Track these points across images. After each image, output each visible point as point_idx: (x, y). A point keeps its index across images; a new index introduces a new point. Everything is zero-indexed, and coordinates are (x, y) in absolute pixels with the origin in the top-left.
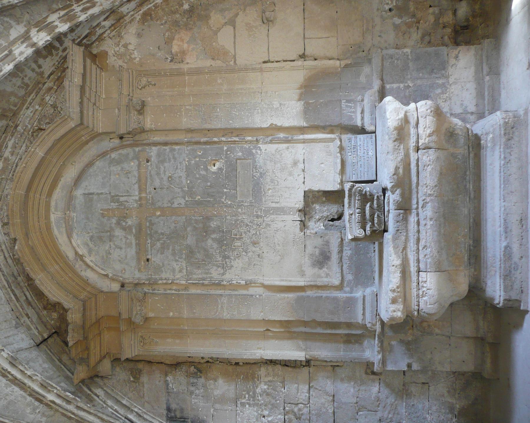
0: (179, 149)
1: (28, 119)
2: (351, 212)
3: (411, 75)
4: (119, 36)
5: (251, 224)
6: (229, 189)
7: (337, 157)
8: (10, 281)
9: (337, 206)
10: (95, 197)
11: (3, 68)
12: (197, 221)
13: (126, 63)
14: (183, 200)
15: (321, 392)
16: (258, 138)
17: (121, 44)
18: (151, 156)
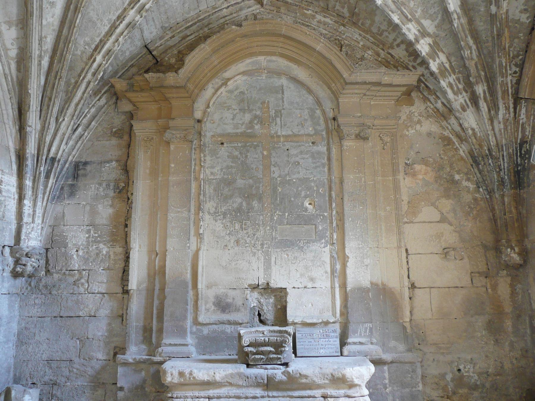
0: (324, 171)
1: (350, 36)
3: (397, 391)
5: (255, 238)
7: (319, 319)
8: (204, 21)
9: (272, 319)
10: (280, 96)
13: (404, 122)
14: (278, 175)
16: (335, 245)
18: (318, 146)
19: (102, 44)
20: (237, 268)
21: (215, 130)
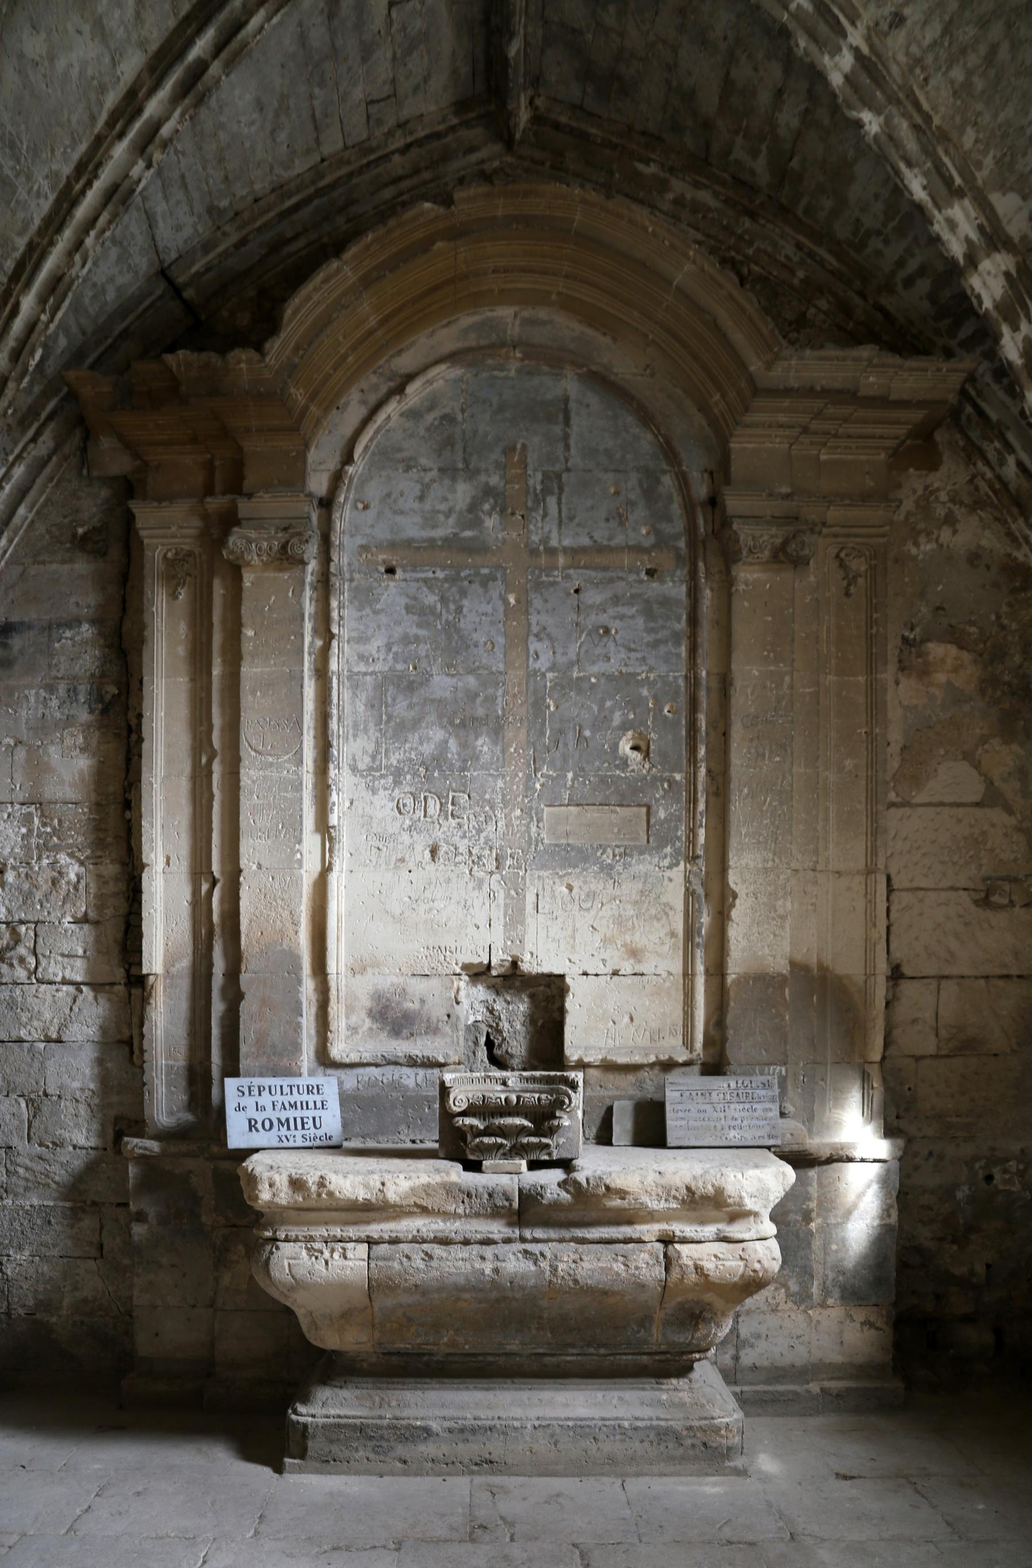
0: (678, 655)
1: (769, 249)
2: (513, 1085)
4: (975, 502)
5: (482, 840)
6: (572, 786)
8: (335, 194)
10: (558, 430)
11: (916, 170)
12: (491, 700)
13: (907, 518)
14: (548, 665)
15: (67, 1012)
16: (701, 862)
17: (956, 508)
18: (662, 581)
19: (35, 256)
20: (432, 920)
21: (368, 531)
